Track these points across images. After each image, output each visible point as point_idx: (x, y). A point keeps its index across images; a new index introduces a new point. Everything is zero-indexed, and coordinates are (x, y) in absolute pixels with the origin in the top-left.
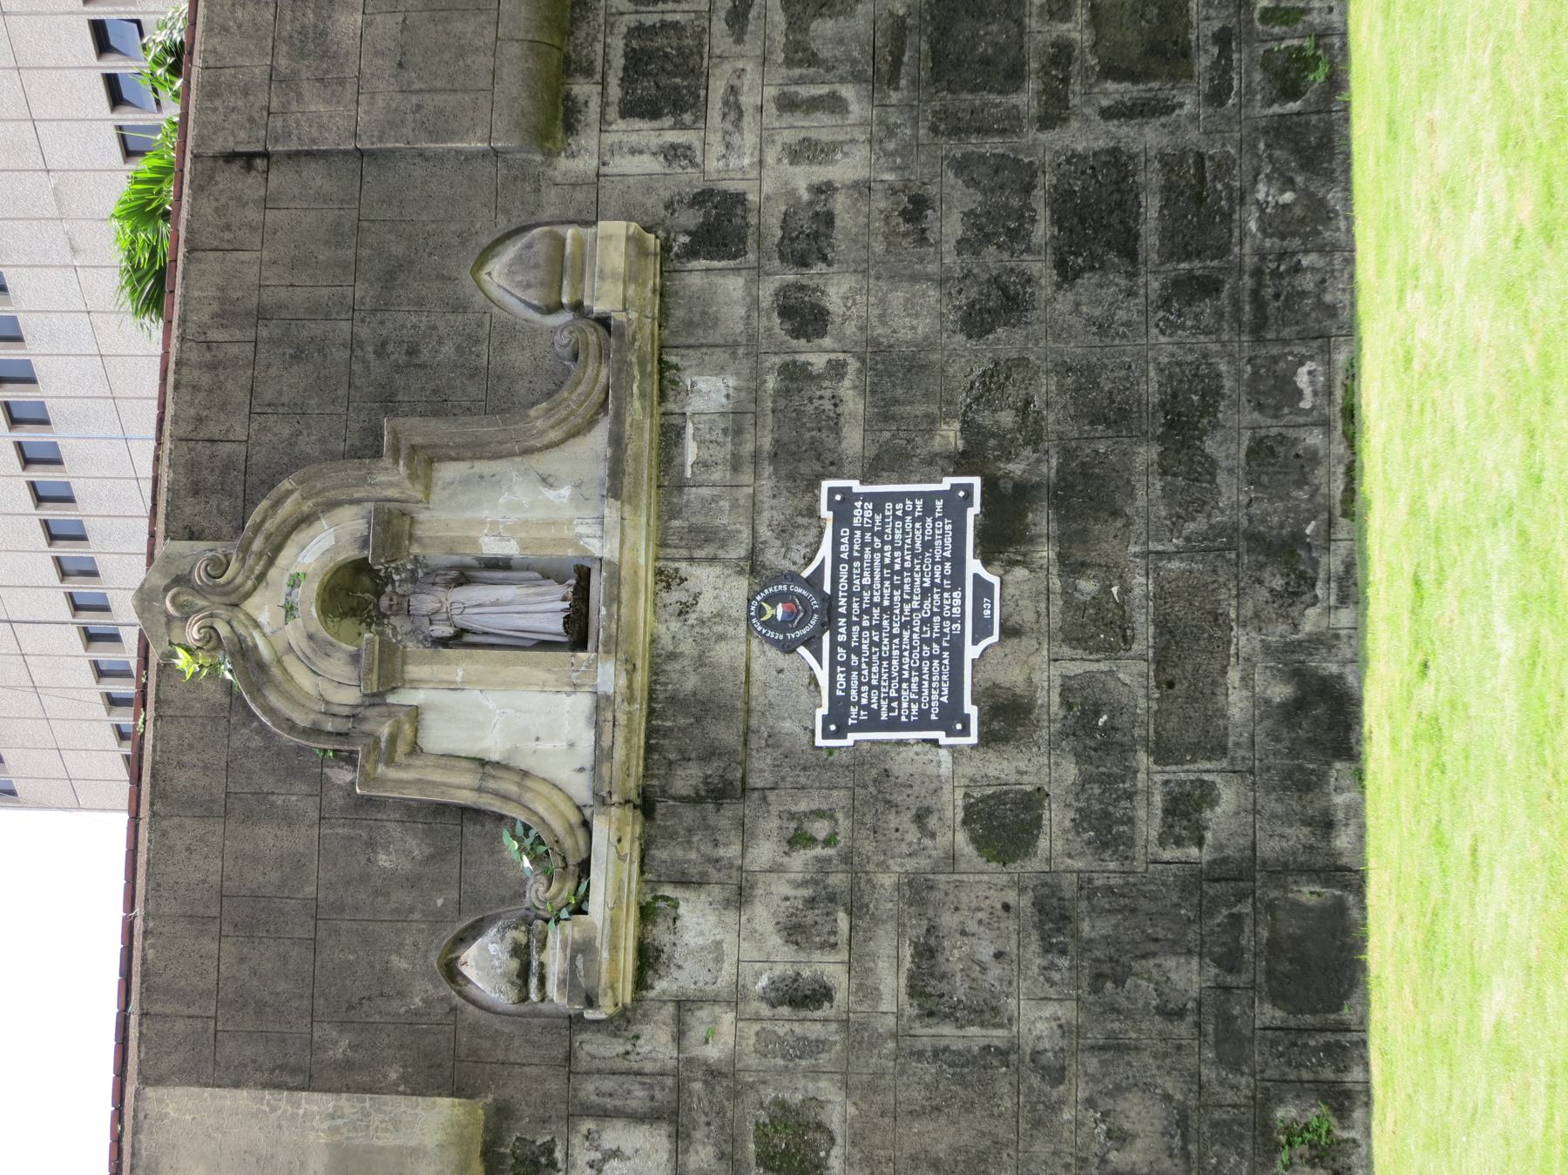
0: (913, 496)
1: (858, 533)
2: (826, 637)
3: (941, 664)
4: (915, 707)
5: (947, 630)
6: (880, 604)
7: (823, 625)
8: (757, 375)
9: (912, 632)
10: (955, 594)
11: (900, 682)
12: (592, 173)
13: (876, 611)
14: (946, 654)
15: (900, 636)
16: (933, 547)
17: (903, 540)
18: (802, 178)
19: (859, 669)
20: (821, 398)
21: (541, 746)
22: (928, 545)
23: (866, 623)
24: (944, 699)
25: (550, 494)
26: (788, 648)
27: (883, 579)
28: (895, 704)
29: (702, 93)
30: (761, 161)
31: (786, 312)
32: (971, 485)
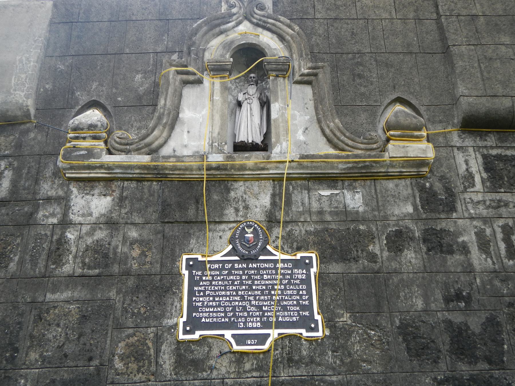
0: (310, 299)
1: (290, 272)
2: (237, 258)
3: (222, 317)
4: (200, 304)
5: (240, 320)
6: (253, 284)
7: (243, 256)
8: (364, 221)
9: (239, 301)
10: (259, 324)
11: (213, 296)
12: (453, 144)
13: (250, 282)
14: (227, 320)
15: (237, 295)
16: (284, 311)
17: (287, 295)
18: (469, 238)
19: (220, 275)
20: (357, 251)
21: (186, 133)
22: (285, 308)
23: (244, 277)
24: (203, 320)
25: (300, 132)
26: (231, 241)
27: (266, 285)
28: (202, 294)
29: (502, 190)
30: (473, 218)
31: (399, 234)
32: (318, 331)
